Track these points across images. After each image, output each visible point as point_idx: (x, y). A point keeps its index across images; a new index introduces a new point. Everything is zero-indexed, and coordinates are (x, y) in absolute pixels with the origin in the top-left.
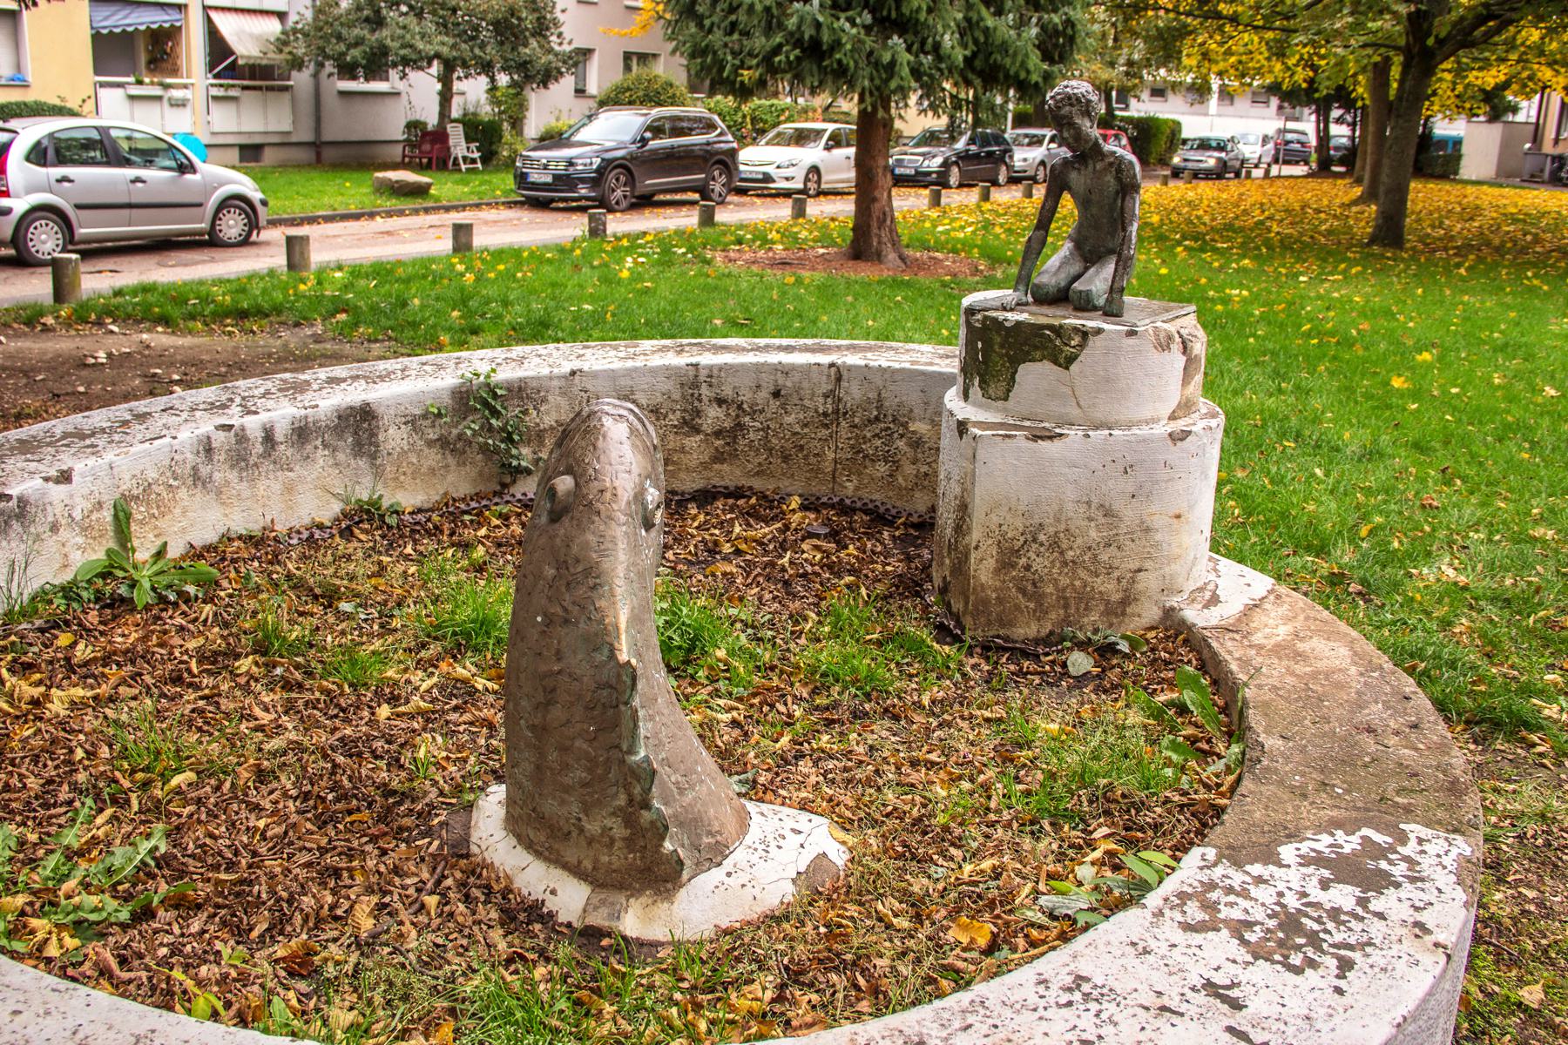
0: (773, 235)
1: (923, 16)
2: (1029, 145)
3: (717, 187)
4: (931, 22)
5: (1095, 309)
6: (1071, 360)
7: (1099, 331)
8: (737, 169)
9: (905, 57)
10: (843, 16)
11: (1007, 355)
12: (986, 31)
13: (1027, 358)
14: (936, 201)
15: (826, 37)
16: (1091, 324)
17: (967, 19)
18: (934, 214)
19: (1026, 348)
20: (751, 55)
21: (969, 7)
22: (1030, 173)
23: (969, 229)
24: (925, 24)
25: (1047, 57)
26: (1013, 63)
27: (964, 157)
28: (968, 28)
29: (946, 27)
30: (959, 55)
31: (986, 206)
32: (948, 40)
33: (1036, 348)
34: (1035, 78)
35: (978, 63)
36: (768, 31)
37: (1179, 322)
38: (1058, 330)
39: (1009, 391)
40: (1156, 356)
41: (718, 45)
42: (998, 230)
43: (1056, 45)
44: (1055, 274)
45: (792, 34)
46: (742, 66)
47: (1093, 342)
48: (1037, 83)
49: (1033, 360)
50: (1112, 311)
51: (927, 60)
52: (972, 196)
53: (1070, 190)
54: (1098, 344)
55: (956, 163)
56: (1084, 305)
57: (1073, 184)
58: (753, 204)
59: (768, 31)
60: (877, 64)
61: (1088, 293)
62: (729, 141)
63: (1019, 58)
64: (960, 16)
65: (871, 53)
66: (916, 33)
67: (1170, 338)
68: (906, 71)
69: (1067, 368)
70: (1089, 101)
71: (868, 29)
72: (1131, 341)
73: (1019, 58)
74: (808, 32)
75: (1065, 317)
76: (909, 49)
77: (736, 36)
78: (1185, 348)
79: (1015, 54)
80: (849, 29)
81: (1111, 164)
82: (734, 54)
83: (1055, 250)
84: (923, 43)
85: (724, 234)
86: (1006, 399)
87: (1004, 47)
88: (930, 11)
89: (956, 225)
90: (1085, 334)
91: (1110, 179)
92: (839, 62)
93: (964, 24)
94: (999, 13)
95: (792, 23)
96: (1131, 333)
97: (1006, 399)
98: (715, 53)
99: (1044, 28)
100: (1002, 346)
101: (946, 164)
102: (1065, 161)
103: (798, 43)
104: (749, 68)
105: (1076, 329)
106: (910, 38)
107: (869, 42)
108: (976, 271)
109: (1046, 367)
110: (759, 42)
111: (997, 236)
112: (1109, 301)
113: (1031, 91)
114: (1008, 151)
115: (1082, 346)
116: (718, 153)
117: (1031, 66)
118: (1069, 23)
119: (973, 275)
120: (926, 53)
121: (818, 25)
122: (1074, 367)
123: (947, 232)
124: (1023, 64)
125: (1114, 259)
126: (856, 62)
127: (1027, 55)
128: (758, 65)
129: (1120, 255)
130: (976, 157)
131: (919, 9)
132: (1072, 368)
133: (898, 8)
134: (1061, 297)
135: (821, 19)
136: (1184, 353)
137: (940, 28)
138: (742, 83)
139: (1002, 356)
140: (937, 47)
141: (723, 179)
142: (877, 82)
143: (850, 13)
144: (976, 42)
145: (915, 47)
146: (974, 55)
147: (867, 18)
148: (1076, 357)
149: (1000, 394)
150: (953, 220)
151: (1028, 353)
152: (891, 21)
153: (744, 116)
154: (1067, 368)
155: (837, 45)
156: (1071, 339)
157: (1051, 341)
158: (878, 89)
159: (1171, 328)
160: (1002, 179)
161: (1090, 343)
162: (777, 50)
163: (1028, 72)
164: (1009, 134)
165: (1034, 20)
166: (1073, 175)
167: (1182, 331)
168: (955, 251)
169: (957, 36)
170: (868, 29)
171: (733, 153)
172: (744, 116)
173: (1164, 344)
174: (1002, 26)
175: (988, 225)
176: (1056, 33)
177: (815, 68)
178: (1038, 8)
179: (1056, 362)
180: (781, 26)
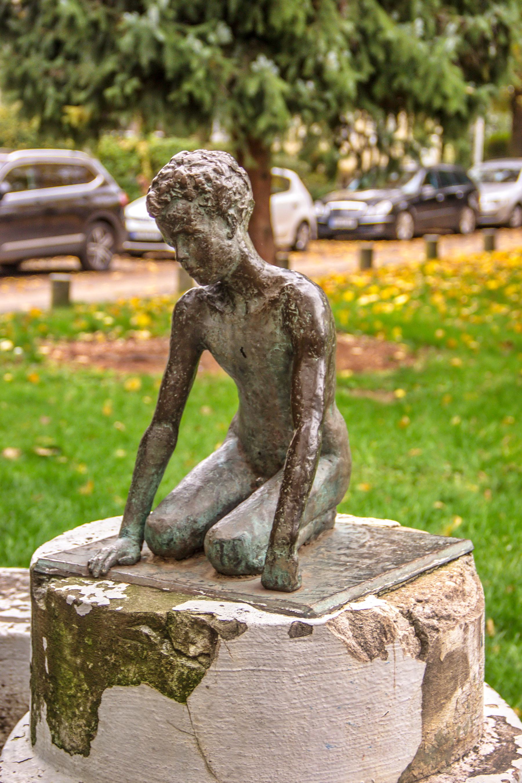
0: (141, 319)
1: (300, 29)
2: (505, 181)
3: (99, 250)
4: (311, 36)
5: (252, 571)
6: (189, 683)
7: (237, 629)
8: (123, 226)
9: (277, 86)
10: (192, 31)
11: (83, 668)
12: (388, 46)
13: (110, 677)
14: (367, 259)
15: (170, 62)
16: (225, 611)
17: (361, 31)
18: (361, 280)
19: (112, 658)
20: (78, 87)
21: (364, 13)
22: (503, 217)
23: (401, 300)
24: (304, 41)
25: (473, 75)
26: (424, 87)
27: (417, 203)
28: (362, 43)
29: (330, 43)
30: (350, 81)
31: (434, 266)
32: (335, 61)
33: (128, 659)
34: (455, 105)
35: (379, 90)
36: (100, 54)
37: (411, 592)
38: (164, 626)
39: (90, 737)
40: (356, 672)
41: (36, 73)
42: (438, 299)
43: (485, 59)
44: (190, 502)
45: (127, 58)
46: (69, 102)
47: (229, 650)
48: (458, 114)
49: (124, 682)
50: (276, 583)
51: (307, 89)
52: (413, 254)
53: (209, 348)
54: (237, 653)
55: (407, 210)
56: (231, 566)
57: (211, 339)
58: (146, 271)
59: (100, 54)
60: (241, 97)
61: (236, 543)
62: (116, 193)
63: (432, 81)
64: (349, 26)
65: (233, 82)
66: (292, 52)
67: (385, 631)
68: (278, 105)
69: (183, 700)
70: (220, 190)
71: (227, 49)
72: (302, 645)
73: (432, 81)
74: (146, 56)
75: (190, 593)
76: (283, 75)
77: (59, 61)
78: (423, 643)
79: (427, 75)
80: (200, 49)
81: (274, 302)
82: (59, 85)
83: (199, 451)
84: (301, 65)
85: (77, 317)
86: (86, 752)
87: (412, 65)
88: (310, 20)
89: (386, 294)
90: (214, 633)
91: (273, 327)
92: (190, 95)
93: (357, 37)
94: (406, 18)
95: (126, 42)
96: (300, 631)
97: (86, 752)
98: (34, 84)
99: (466, 36)
100: (75, 652)
101: (395, 213)
102: (201, 300)
103: (136, 70)
104: (78, 104)
105: (199, 625)
106: (284, 59)
107: (229, 67)
108: (390, 361)
109: (146, 695)
110: (89, 70)
111: (435, 309)
112: (271, 561)
113: (454, 123)
114: (473, 191)
115: (209, 655)
116: (98, 208)
117: (448, 89)
118: (501, 28)
119: (385, 366)
120: (305, 79)
121: (159, 46)
122: (196, 698)
123: (370, 305)
124: (438, 88)
125: (279, 480)
126: (213, 95)
127: (442, 76)
128: (87, 101)
129: (288, 473)
130: (433, 202)
131: (294, 20)
132: (191, 699)
133: (266, 19)
134: (191, 549)
135: (161, 36)
136: (421, 655)
137: (322, 45)
138: (69, 124)
139: (76, 670)
140: (319, 71)
141: (107, 241)
142: (242, 120)
143: (202, 28)
144: (373, 60)
145: (292, 71)
146: (373, 78)
147: (223, 33)
148: (200, 676)
149: (77, 741)
150: (382, 287)
151: (115, 667)
152: (259, 36)
153: (140, 161)
154: (183, 700)
155: (185, 72)
156: (188, 641)
157: (152, 646)
158: (244, 129)
159: (387, 608)
160: (466, 224)
161: (222, 652)
162: (109, 80)
163: (445, 98)
164: (475, 173)
165: (452, 27)
166: (212, 322)
167: (419, 611)
168: (371, 333)
169: (347, 54)
170: (227, 49)
171: (118, 209)
172: (140, 161)
173: (374, 643)
174: (406, 36)
175: (426, 293)
176: (485, 43)
177: (160, 105)
178: (462, 9)
179: (163, 687)
180: (114, 48)
